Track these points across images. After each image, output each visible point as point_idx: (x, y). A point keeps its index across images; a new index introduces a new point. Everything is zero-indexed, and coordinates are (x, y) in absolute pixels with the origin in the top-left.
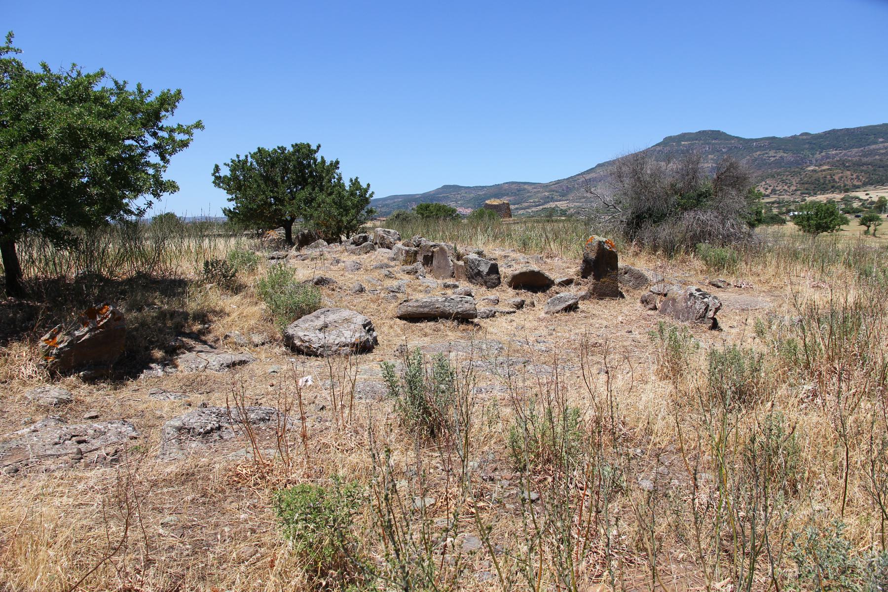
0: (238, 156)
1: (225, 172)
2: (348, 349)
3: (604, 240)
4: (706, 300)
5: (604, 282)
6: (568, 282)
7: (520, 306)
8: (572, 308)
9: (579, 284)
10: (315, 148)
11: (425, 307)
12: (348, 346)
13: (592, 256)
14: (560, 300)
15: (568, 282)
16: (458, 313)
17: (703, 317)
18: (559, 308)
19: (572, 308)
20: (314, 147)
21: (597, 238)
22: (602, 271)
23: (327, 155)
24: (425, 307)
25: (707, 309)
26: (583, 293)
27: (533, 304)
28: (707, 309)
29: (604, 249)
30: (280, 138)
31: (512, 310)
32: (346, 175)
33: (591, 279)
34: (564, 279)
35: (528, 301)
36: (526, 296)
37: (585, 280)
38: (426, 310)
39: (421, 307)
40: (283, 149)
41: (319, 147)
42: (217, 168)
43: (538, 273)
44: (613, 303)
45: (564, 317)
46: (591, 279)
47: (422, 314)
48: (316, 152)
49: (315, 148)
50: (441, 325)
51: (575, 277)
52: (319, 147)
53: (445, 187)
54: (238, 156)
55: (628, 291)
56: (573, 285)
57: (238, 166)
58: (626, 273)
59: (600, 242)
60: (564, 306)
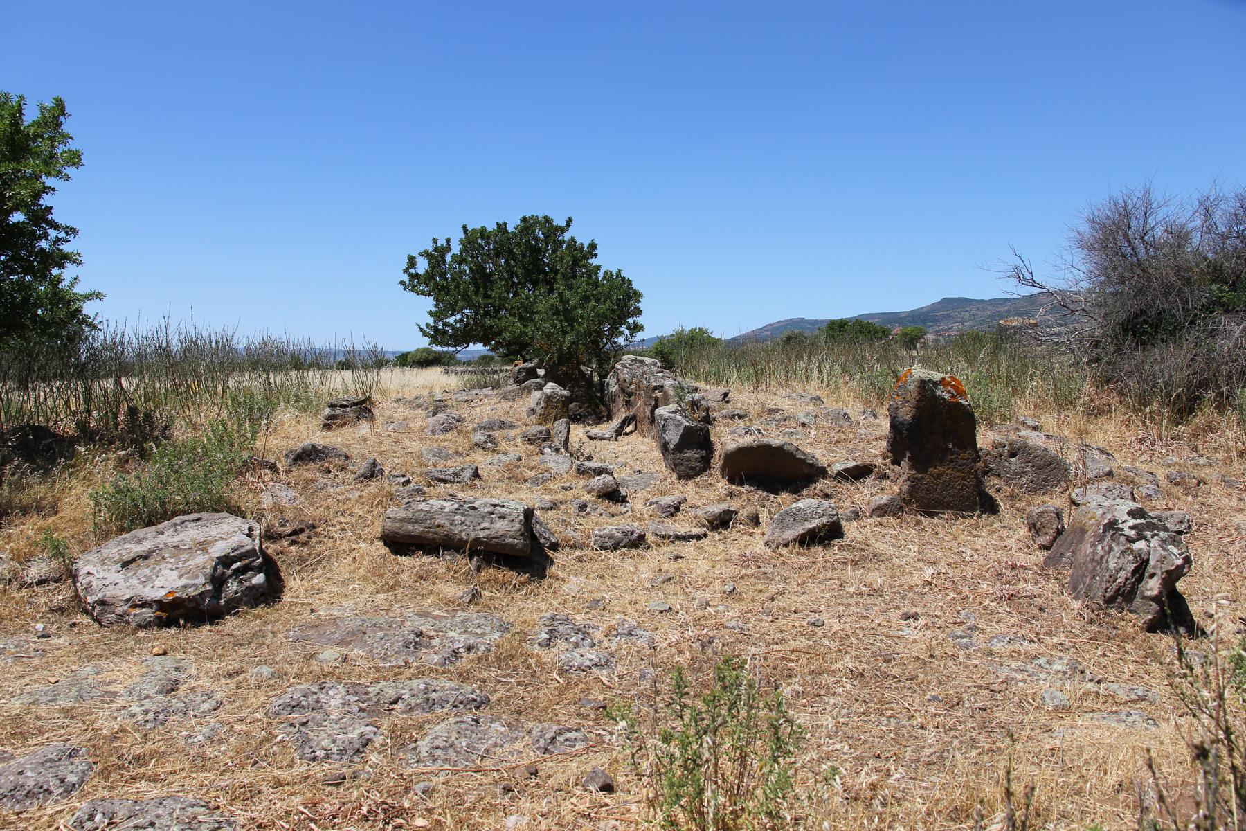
0: (435, 241)
1: (422, 266)
2: (147, 613)
3: (937, 376)
4: (1140, 545)
5: (939, 476)
6: (859, 473)
7: (722, 522)
8: (829, 534)
9: (883, 477)
10: (563, 224)
11: (417, 521)
12: (150, 606)
13: (906, 414)
14: (797, 516)
15: (859, 473)
16: (477, 541)
17: (1124, 596)
18: (790, 534)
19: (829, 534)
20: (559, 222)
21: (919, 372)
22: (940, 456)
23: (580, 234)
24: (417, 521)
25: (1141, 570)
26: (883, 499)
27: (755, 520)
28: (1141, 570)
29: (935, 399)
30: (503, 211)
31: (696, 531)
32: (606, 262)
33: (904, 468)
34: (851, 464)
35: (743, 514)
36: (748, 500)
37: (897, 468)
38: (418, 529)
39: (409, 521)
40: (502, 227)
41: (569, 221)
42: (412, 261)
43: (780, 449)
44: (961, 526)
45: (797, 557)
46: (904, 468)
47: (409, 536)
48: (563, 230)
49: (563, 224)
50: (440, 565)
51: (878, 461)
52: (569, 221)
53: (946, 301)
54: (435, 241)
55: (1013, 497)
56: (869, 480)
57: (437, 255)
58: (1013, 455)
59: (923, 384)
60: (799, 530)
